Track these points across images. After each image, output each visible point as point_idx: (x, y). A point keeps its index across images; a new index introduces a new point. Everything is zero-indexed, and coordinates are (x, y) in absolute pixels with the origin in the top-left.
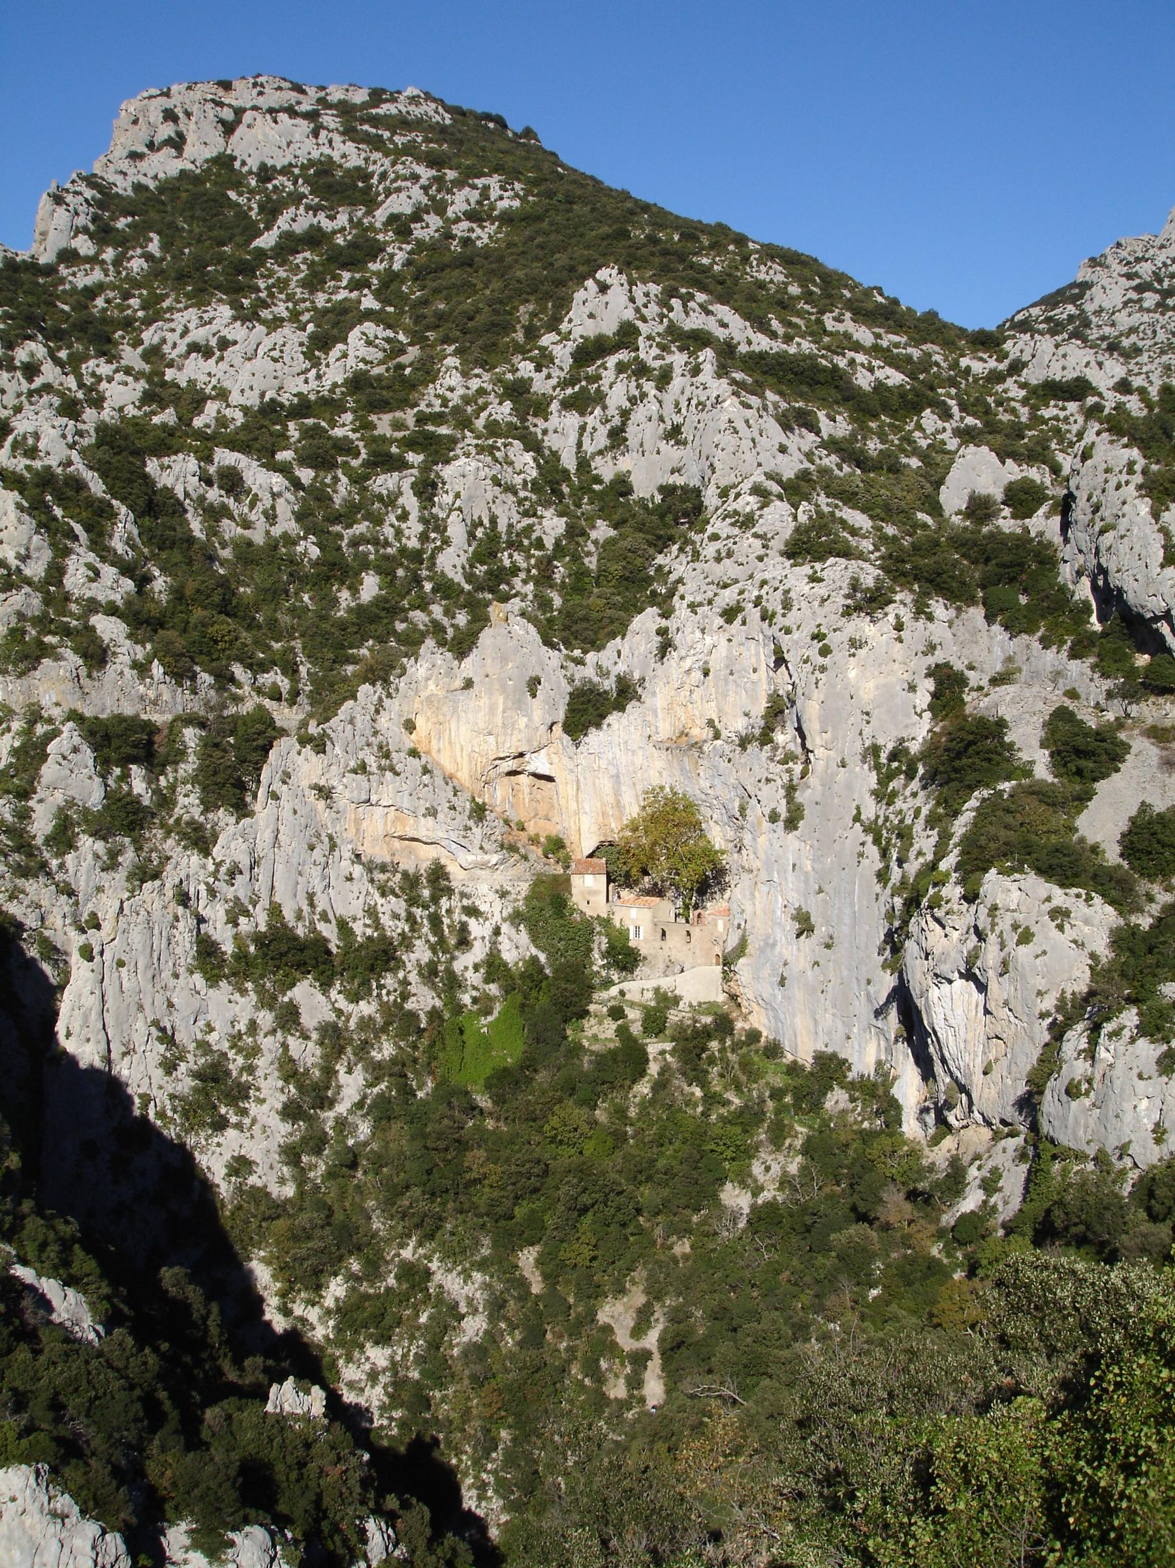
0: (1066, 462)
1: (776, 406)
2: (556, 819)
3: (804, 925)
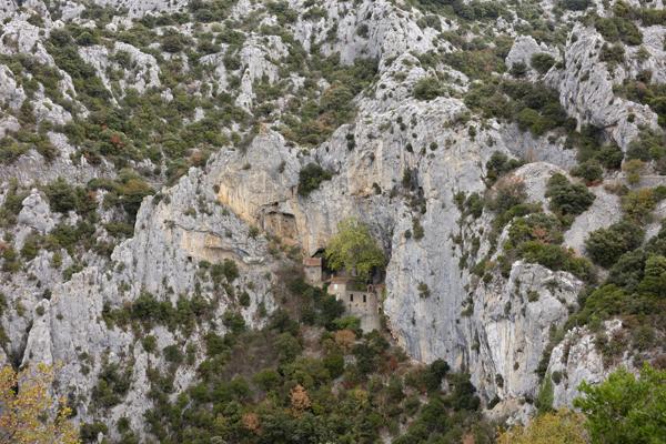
1: (417, 16)
2: (295, 237)
3: (425, 292)
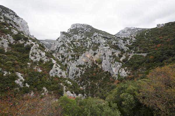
0: (119, 41)
3: (106, 64)
